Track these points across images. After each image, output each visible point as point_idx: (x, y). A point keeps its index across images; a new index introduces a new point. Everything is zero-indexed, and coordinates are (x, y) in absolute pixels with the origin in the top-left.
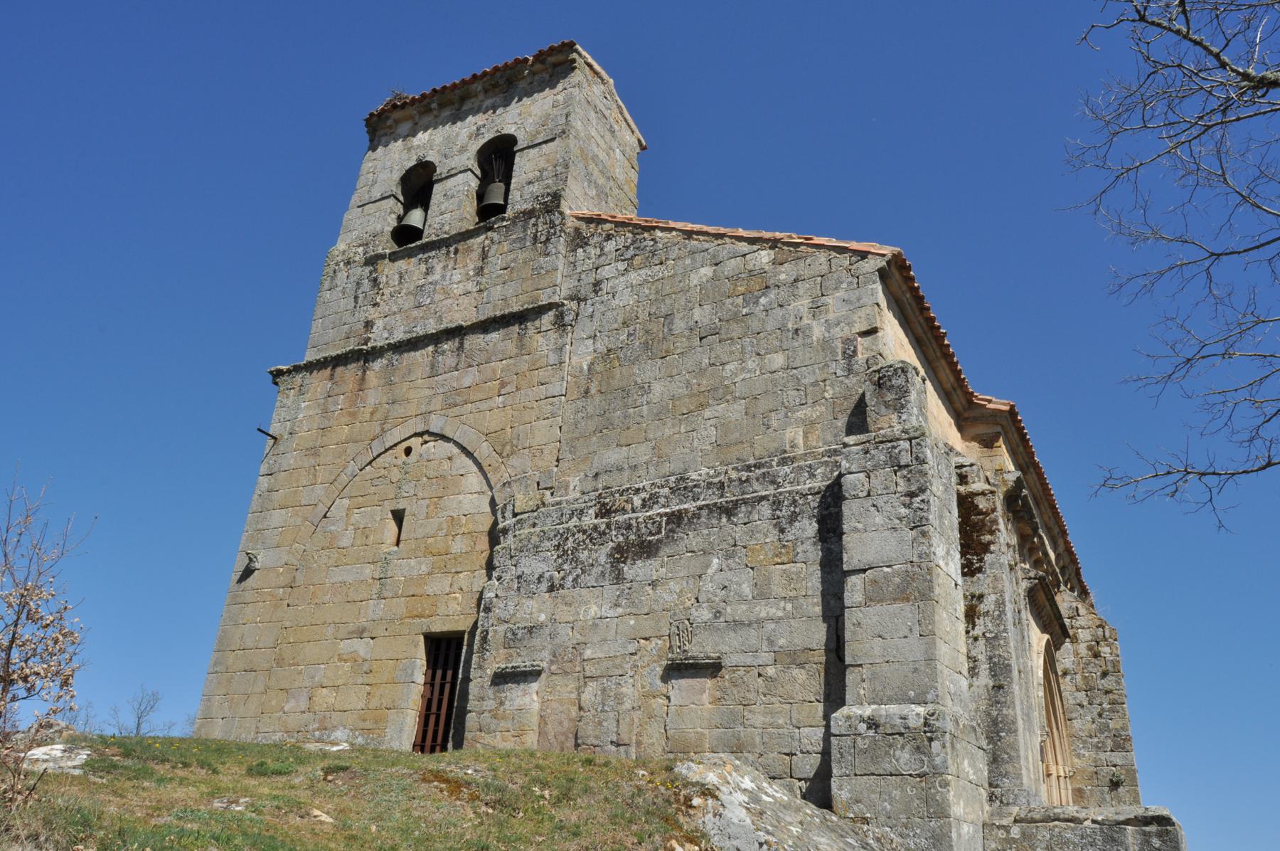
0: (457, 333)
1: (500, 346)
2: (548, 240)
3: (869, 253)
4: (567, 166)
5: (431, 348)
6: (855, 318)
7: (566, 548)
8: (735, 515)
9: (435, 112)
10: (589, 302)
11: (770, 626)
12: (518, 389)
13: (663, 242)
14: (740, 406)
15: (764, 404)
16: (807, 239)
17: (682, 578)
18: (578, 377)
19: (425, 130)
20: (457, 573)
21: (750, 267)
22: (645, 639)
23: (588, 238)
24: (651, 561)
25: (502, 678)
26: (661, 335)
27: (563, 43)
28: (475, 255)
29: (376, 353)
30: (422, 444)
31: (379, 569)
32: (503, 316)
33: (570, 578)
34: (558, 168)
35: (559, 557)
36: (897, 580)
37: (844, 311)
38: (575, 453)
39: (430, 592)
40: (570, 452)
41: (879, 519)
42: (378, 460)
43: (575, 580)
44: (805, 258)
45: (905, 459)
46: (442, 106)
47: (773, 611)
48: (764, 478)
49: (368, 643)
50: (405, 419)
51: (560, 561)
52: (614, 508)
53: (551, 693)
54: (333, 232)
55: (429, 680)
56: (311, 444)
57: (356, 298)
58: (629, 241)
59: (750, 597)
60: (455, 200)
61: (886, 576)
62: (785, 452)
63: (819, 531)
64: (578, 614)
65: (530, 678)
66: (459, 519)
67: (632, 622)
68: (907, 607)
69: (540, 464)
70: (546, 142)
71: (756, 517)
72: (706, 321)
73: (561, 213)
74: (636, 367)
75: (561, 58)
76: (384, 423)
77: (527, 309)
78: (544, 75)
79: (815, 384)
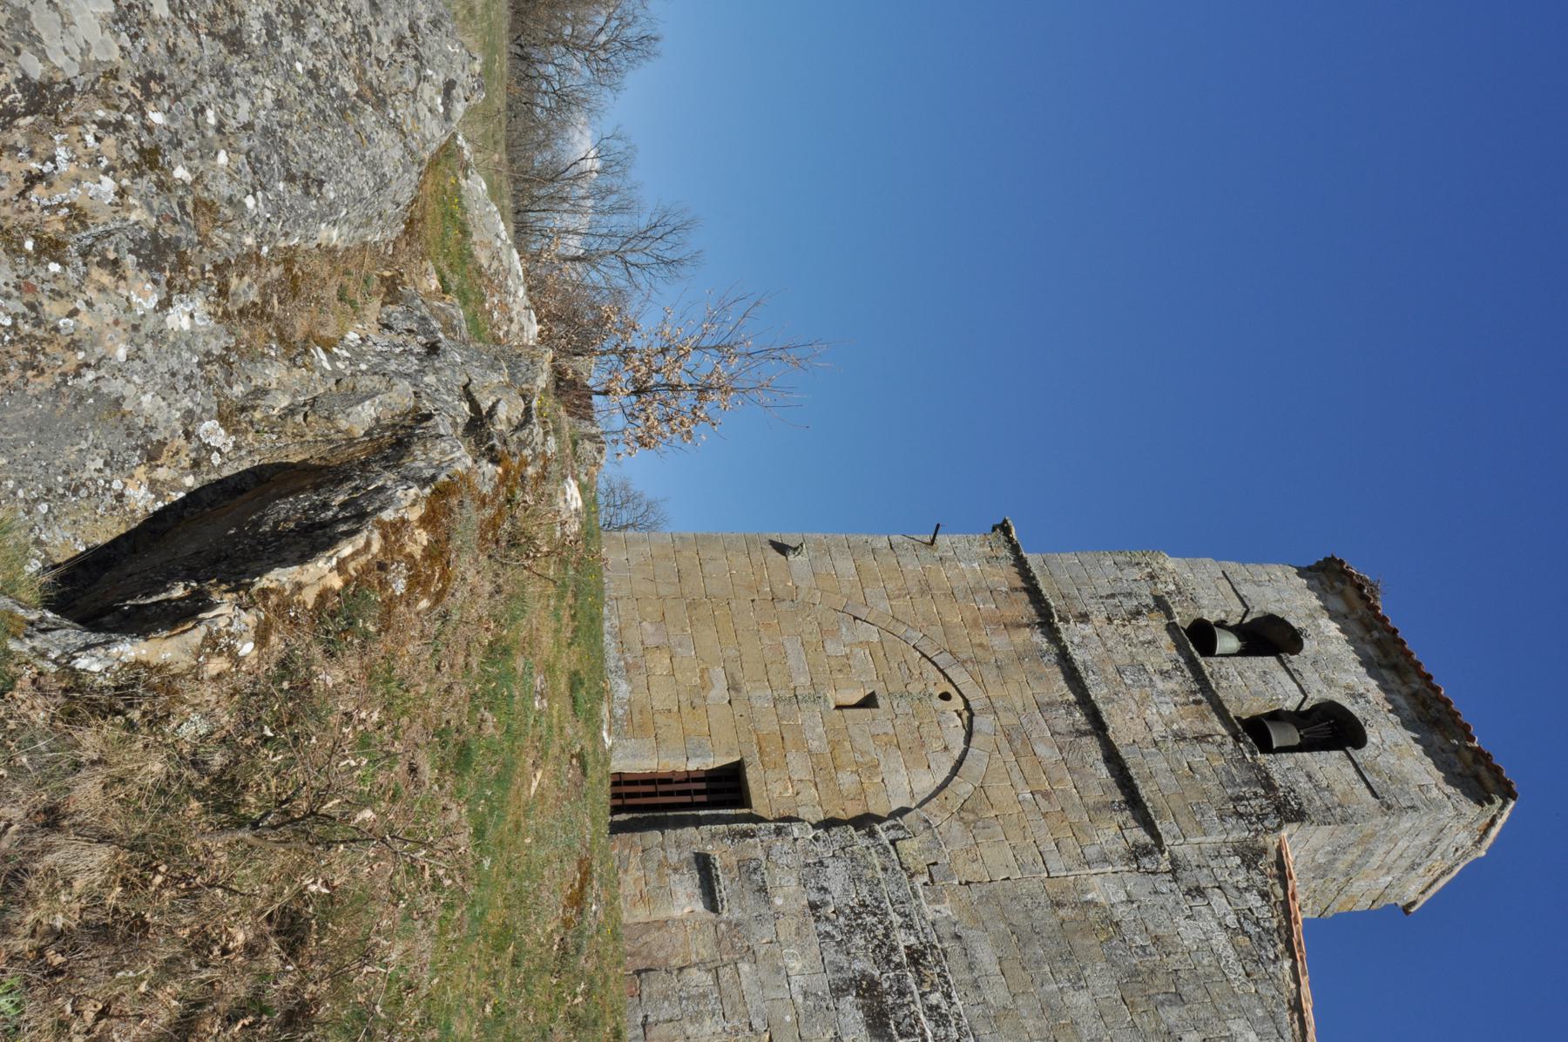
0: (1098, 726)
1: (1093, 782)
2: (1241, 816)
5: (1072, 697)
7: (864, 915)
9: (1367, 637)
10: (1174, 885)
12: (1045, 815)
19: (1342, 630)
20: (816, 785)
23: (1257, 868)
25: (704, 864)
27: (1510, 783)
28: (1199, 727)
29: (1052, 634)
32: (1130, 779)
33: (829, 928)
34: (1339, 809)
35: (852, 908)
39: (790, 757)
40: (981, 897)
43: (828, 935)
46: (1378, 643)
49: (723, 698)
50: (981, 684)
51: (848, 911)
52: (922, 969)
55: (692, 776)
56: (933, 584)
57: (1113, 596)
58: (1267, 924)
60: (1261, 686)
64: (788, 947)
65: (708, 900)
67: (788, 1018)
69: (960, 861)
70: (1369, 786)
77: (1146, 807)
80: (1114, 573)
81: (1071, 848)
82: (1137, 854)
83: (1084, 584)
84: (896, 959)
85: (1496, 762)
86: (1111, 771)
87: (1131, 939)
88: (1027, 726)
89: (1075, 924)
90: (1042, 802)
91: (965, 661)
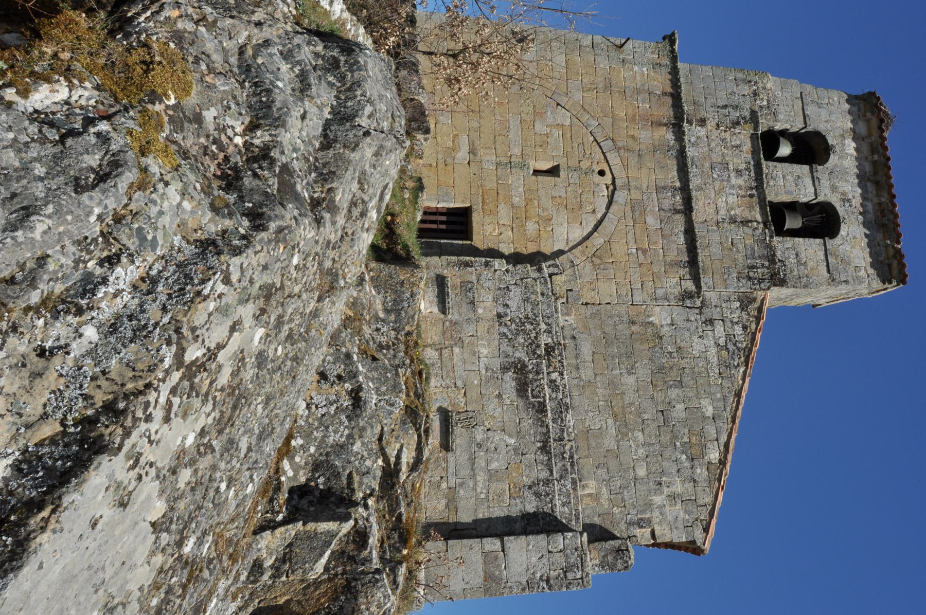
0: (688, 208)
1: (674, 247)
2: (750, 278)
3: (707, 534)
4: (805, 286)
5: (678, 184)
6: (664, 526)
7: (526, 324)
8: (542, 453)
9: (870, 158)
10: (699, 316)
11: (471, 484)
12: (640, 265)
13: (736, 373)
14: (613, 445)
15: (613, 463)
16: (723, 487)
17: (503, 418)
18: (644, 314)
19: (857, 150)
20: (512, 229)
21: (709, 445)
22: (465, 393)
23: (747, 310)
24: (515, 394)
25: (441, 282)
26: (668, 379)
27: (907, 276)
28: (748, 215)
29: (679, 134)
30: (606, 184)
31: (517, 160)
32: (696, 248)
33: (506, 331)
34: (805, 278)
35: (520, 319)
36: (497, 573)
37: (670, 517)
38: (590, 318)
39: (500, 208)
40: (592, 314)
41: (534, 559)
42: (597, 147)
43: (504, 335)
44: (709, 487)
45: (570, 576)
46: (874, 163)
47: (480, 485)
48: (564, 470)
49: (465, 159)
50: (626, 167)
51: (518, 321)
52: (551, 358)
53: (431, 323)
54: (783, 72)
55: (439, 211)
56: (614, 82)
57: (725, 107)
58: (740, 345)
59: (489, 468)
60: (793, 188)
61: (499, 565)
62: (580, 481)
63: (529, 514)
64: (482, 340)
65: (441, 306)
66: (550, 226)
67: (476, 382)
68: (481, 580)
69: (585, 289)
70: (828, 266)
71: (539, 468)
72: (674, 414)
73: (769, 288)
74: (647, 362)
75: (895, 272)
76: (624, 149)
77: (699, 268)
78: (883, 256)
79: (623, 500)
80: (732, 87)
81: (650, 288)
82: (686, 295)
83: (710, 94)
84: (538, 352)
85: (905, 261)
86: (686, 240)
87: (666, 347)
88: (646, 202)
89: (638, 336)
90: (641, 256)
91: (620, 148)
